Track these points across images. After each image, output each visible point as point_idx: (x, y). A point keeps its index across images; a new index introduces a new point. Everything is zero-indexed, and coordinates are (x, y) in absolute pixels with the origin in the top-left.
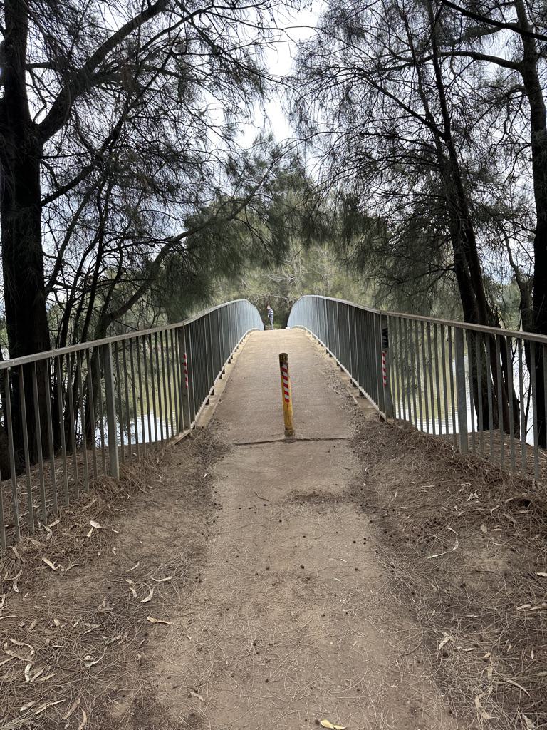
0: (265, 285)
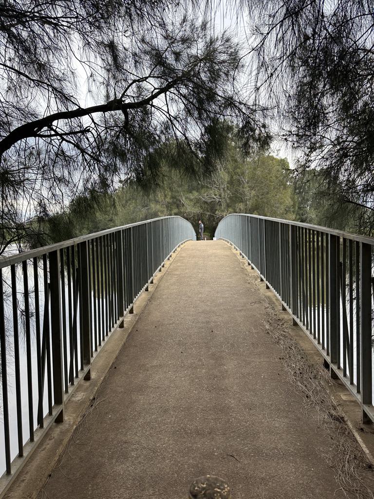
0: (198, 205)
